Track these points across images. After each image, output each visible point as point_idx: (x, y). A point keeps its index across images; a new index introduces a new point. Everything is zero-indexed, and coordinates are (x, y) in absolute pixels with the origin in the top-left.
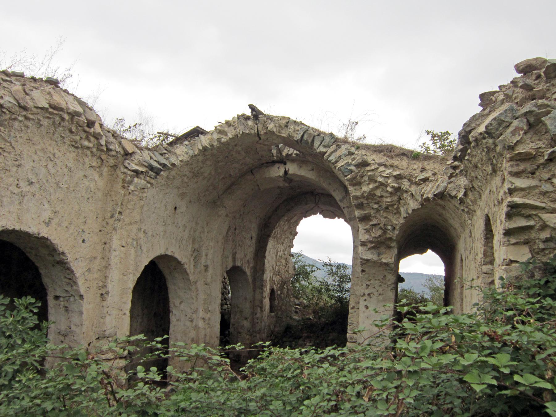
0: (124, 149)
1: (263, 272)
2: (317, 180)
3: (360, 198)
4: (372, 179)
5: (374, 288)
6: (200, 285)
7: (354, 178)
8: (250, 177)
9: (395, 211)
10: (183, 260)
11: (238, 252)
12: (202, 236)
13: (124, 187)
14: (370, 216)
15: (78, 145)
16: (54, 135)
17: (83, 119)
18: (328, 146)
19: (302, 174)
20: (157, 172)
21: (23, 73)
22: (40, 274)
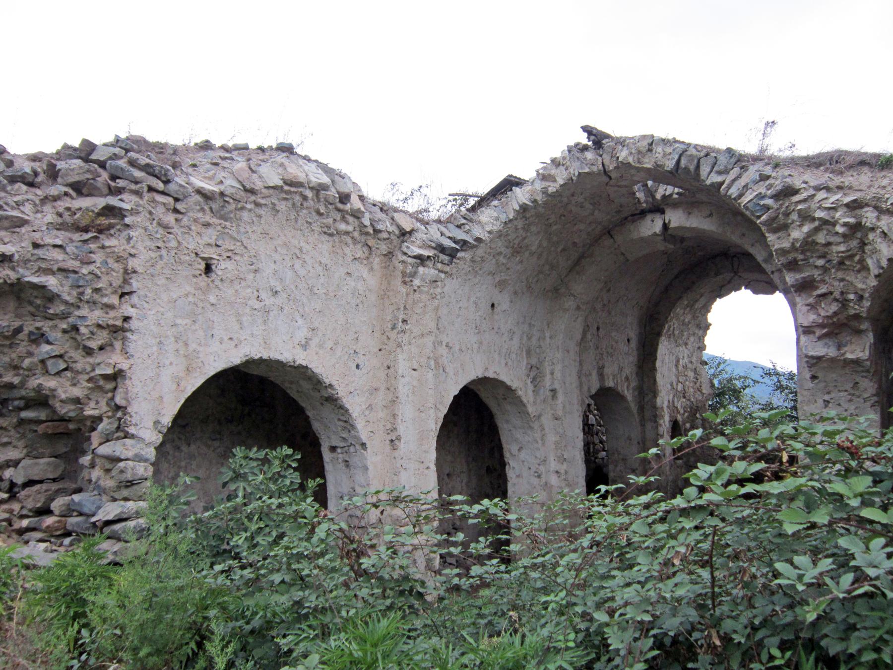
0: (398, 226)
1: (655, 393)
2: (720, 230)
3: (789, 252)
4: (806, 217)
5: (839, 405)
6: (547, 421)
7: (773, 219)
8: (608, 242)
9: (859, 266)
10: (514, 384)
11: (607, 365)
12: (542, 344)
13: (405, 283)
14: (814, 280)
15: (332, 230)
16: (296, 222)
17: (332, 192)
18: (726, 172)
19: (694, 225)
20: (452, 254)
21: (247, 144)
22: (308, 417)
